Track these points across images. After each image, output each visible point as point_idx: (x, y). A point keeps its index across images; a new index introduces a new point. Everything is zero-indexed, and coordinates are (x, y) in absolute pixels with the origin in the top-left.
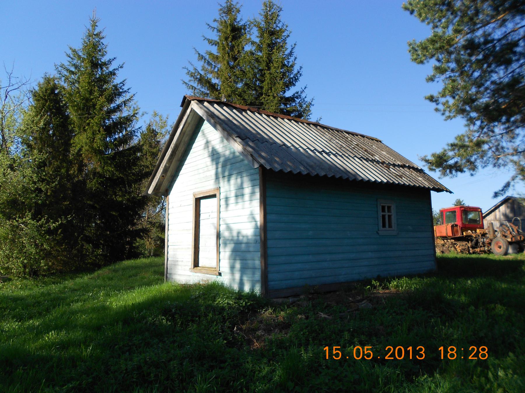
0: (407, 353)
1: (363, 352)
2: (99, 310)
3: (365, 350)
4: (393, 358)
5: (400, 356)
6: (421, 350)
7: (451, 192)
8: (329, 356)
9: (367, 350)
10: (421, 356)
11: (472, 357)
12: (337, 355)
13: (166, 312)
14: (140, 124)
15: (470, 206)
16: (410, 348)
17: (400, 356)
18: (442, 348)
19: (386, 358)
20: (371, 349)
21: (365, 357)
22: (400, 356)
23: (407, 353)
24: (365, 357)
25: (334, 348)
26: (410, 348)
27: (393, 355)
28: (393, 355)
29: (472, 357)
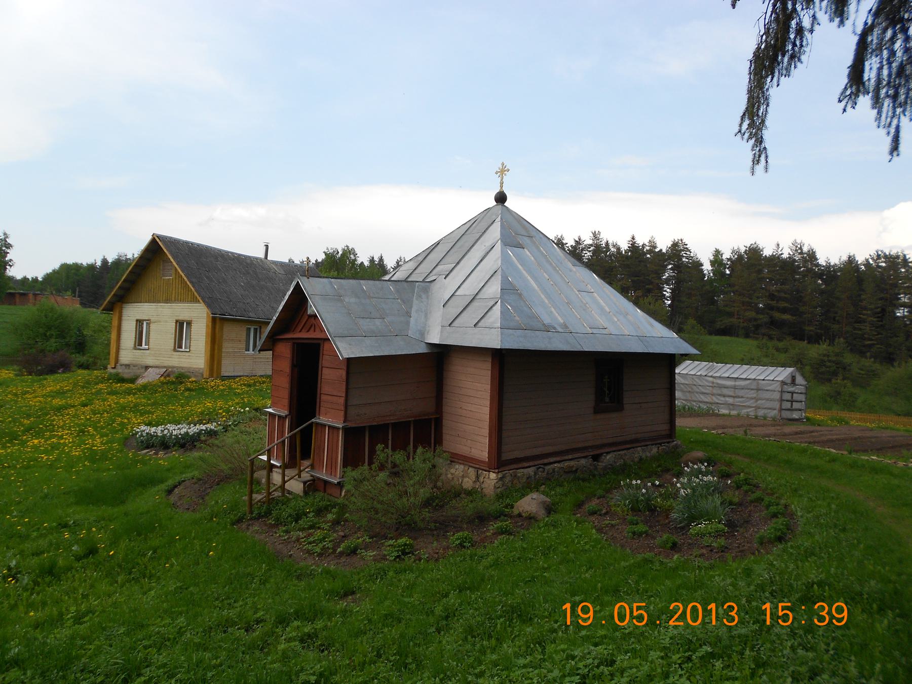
1: (631, 612)
3: (635, 609)
5: (695, 619)
7: (760, 153)
8: (771, 614)
10: (821, 619)
12: (785, 618)
13: (524, 227)
15: (85, 259)
16: (713, 606)
17: (695, 620)
20: (646, 609)
21: (634, 621)
22: (695, 619)
24: (834, 621)
25: (780, 605)
26: (713, 606)
28: (683, 616)
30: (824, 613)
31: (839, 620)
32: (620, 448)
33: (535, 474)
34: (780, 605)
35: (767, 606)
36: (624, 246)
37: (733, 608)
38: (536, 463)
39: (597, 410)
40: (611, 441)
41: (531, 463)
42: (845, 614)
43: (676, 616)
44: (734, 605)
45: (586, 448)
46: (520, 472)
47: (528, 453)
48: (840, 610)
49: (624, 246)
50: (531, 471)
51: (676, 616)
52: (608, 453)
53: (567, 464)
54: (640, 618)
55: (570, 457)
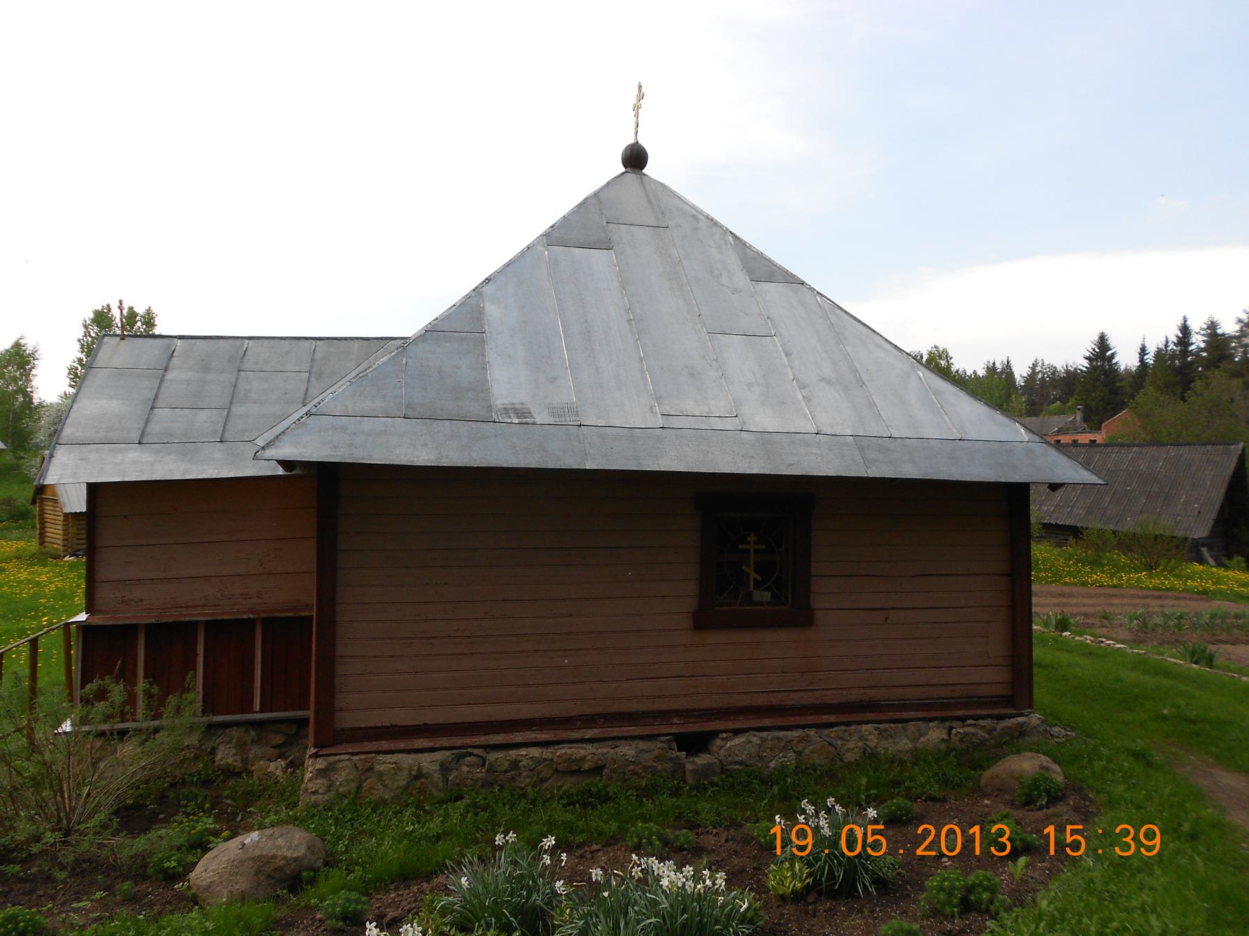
0: (969, 841)
2: (858, 764)
4: (934, 853)
6: (1001, 833)
8: (1056, 844)
9: (873, 834)
11: (925, 849)
12: (1076, 846)
14: (1122, 368)
16: (976, 829)
18: (1050, 830)
19: (919, 852)
21: (869, 850)
23: (969, 841)
24: (1142, 850)
25: (1069, 827)
26: (976, 829)
27: (935, 844)
28: (935, 844)
29: (925, 849)
30: (1128, 839)
31: (1149, 849)
32: (792, 721)
33: (445, 768)
34: (1069, 827)
35: (1050, 830)
36: (981, 373)
37: (1128, 833)
38: (459, 741)
39: (703, 621)
40: (762, 701)
41: (444, 742)
42: (1158, 839)
43: (926, 843)
44: (1005, 827)
45: (664, 716)
46: (384, 763)
47: (525, 711)
48: (1150, 835)
49: (981, 373)
50: (429, 762)
51: (926, 843)
52: (737, 732)
53: (562, 751)
54: (876, 845)
55: (589, 734)
